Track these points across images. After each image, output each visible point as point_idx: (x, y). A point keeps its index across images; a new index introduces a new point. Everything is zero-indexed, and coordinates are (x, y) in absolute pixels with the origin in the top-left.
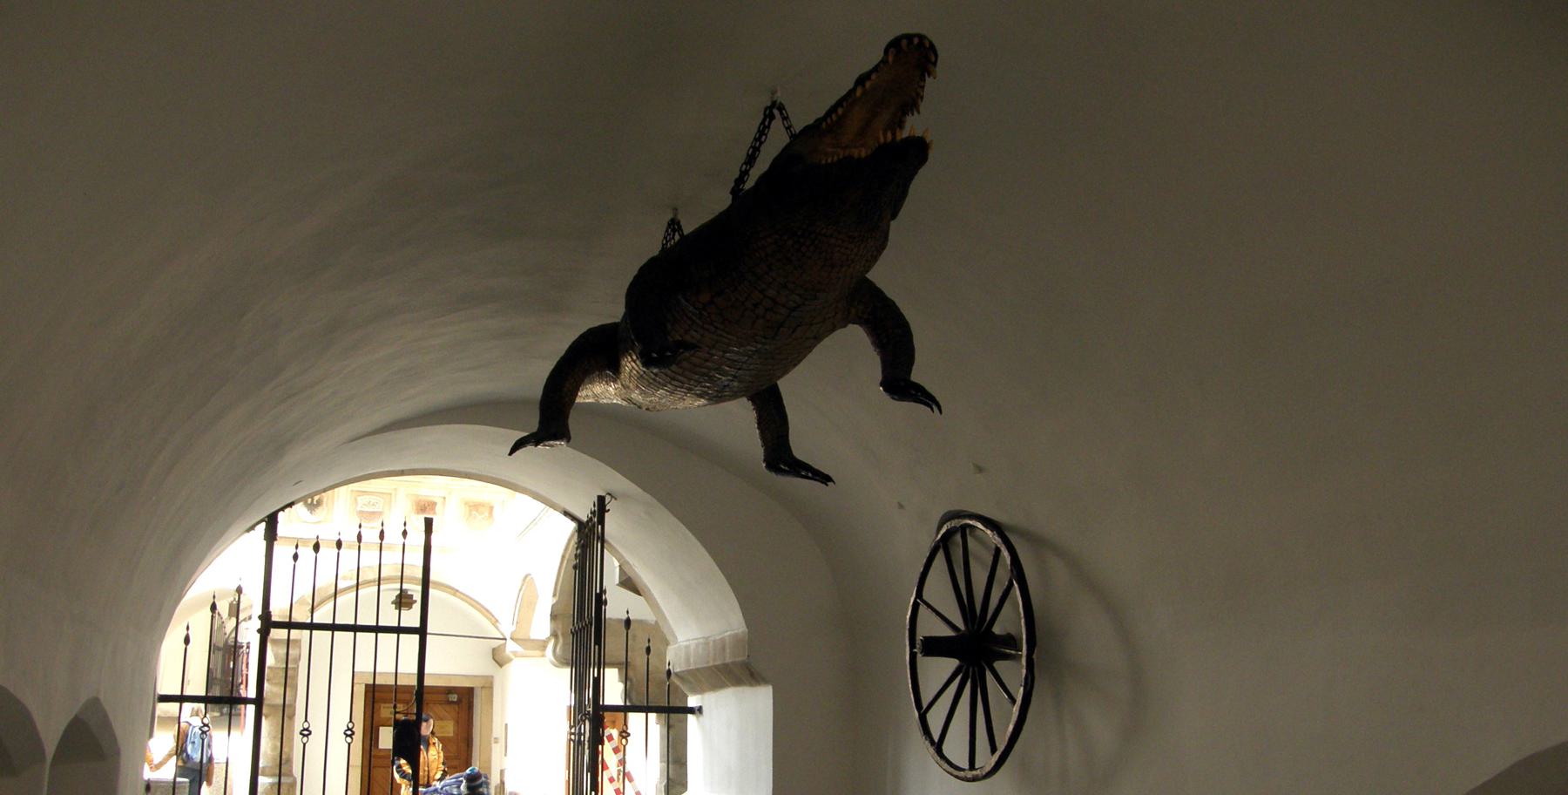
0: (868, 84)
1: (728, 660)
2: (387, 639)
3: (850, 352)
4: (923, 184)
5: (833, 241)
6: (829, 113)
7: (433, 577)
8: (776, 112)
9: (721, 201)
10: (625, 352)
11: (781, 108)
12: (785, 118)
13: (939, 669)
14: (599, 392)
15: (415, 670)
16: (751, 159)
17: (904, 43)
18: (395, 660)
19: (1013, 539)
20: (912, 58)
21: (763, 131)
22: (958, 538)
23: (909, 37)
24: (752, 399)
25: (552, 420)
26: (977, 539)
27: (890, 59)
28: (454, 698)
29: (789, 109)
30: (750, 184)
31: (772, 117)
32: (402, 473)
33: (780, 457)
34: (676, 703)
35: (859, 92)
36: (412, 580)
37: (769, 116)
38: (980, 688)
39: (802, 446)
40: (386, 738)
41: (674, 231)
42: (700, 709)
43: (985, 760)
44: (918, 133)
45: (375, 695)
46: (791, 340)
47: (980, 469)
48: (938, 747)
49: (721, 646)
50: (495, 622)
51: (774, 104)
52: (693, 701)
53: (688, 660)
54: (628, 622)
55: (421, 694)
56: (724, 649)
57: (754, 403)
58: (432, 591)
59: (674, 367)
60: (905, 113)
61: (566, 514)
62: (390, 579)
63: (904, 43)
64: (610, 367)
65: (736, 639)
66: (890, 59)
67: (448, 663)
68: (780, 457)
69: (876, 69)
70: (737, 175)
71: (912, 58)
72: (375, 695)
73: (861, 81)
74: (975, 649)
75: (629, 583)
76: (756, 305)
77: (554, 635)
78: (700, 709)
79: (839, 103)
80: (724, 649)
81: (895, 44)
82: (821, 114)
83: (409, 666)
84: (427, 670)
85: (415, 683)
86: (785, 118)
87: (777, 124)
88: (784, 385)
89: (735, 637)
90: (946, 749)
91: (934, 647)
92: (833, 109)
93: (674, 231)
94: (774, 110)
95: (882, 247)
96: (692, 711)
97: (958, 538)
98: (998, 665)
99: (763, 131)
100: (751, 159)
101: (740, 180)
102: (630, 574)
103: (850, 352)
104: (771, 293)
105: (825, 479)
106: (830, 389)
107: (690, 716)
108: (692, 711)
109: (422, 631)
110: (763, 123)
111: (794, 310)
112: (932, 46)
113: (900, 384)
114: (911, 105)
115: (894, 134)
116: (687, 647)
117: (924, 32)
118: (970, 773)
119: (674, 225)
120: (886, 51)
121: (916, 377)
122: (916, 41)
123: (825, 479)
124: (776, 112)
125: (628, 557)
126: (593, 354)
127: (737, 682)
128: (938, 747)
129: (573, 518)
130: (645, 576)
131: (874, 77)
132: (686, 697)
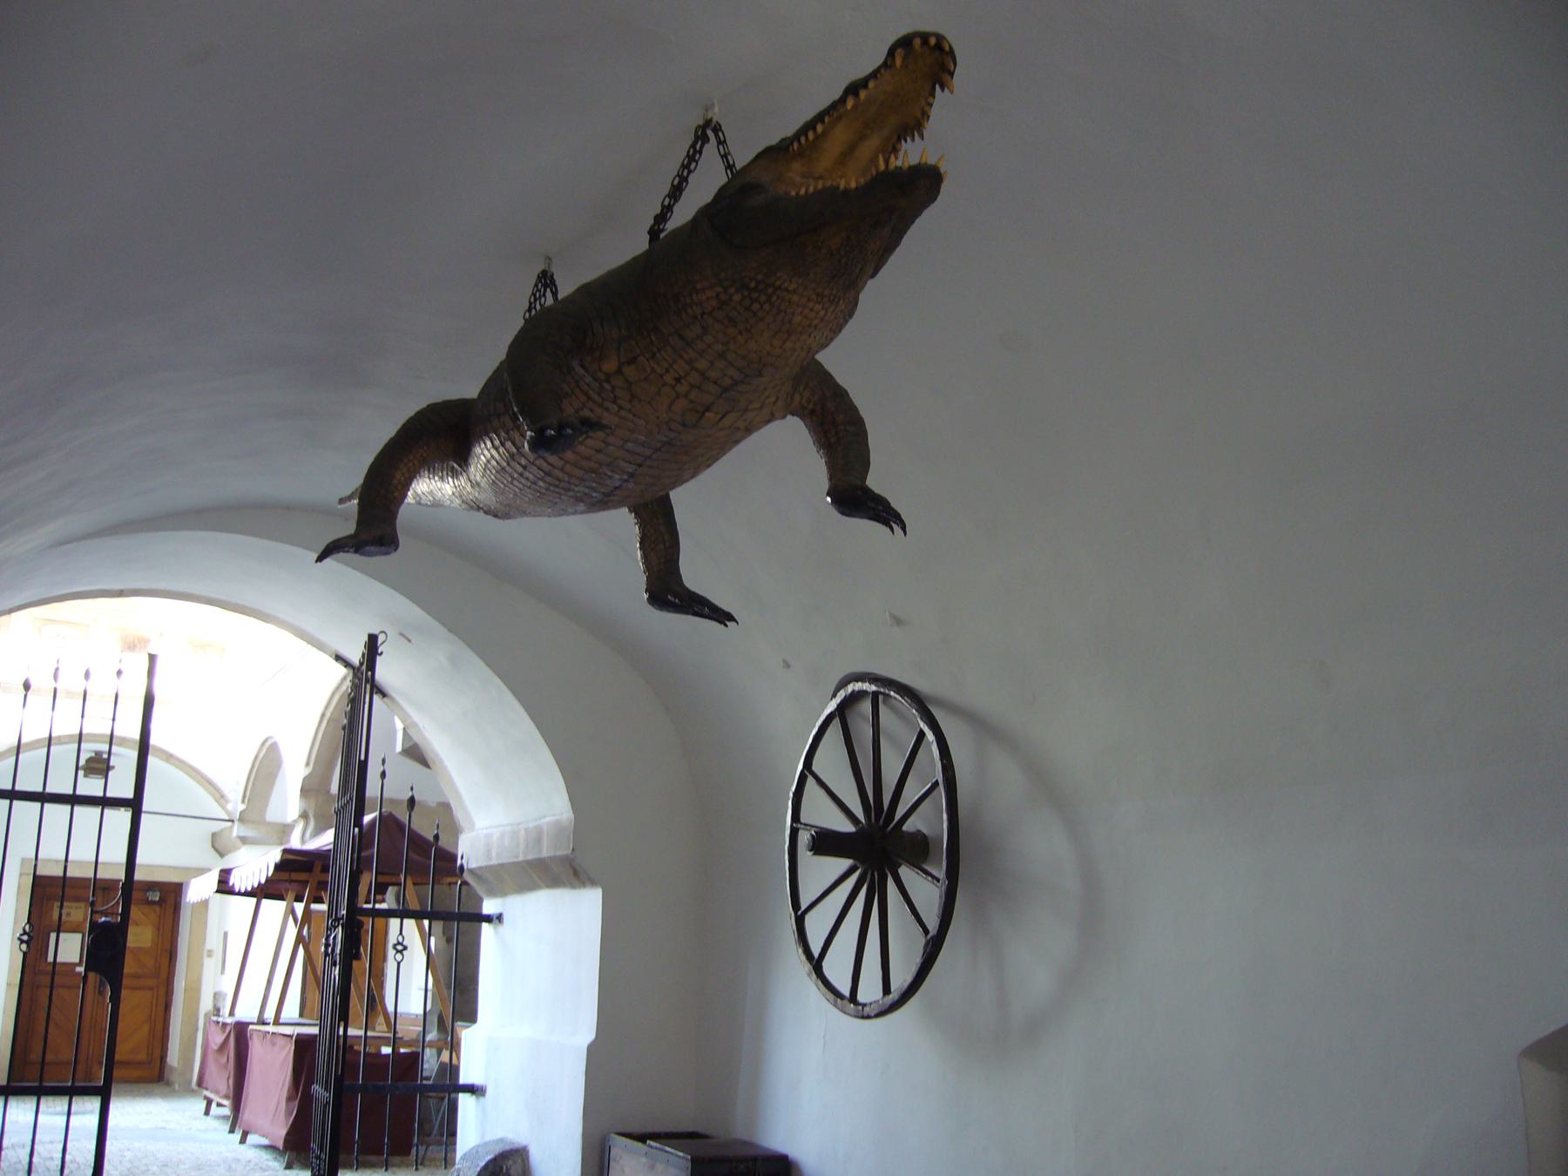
0: (863, 94)
1: (545, 853)
2: (87, 816)
3: (785, 452)
4: (927, 232)
5: (795, 298)
6: (797, 136)
7: (154, 740)
8: (710, 133)
9: (627, 244)
10: (480, 438)
11: (717, 129)
12: (721, 143)
13: (821, 871)
14: (431, 489)
15: (123, 858)
16: (676, 192)
17: (917, 42)
18: (91, 845)
19: (938, 714)
20: (924, 61)
21: (693, 157)
22: (866, 706)
23: (924, 37)
24: (635, 510)
25: (373, 527)
26: (892, 708)
27: (898, 62)
28: (155, 896)
29: (729, 132)
30: (682, 215)
31: (705, 140)
32: (121, 594)
33: (668, 591)
34: (50, 968)
35: (850, 103)
36: (124, 742)
37: (701, 137)
38: (877, 893)
39: (695, 574)
40: (70, 949)
41: (546, 286)
42: (500, 918)
43: (870, 990)
44: (931, 161)
45: (50, 895)
46: (697, 440)
47: (898, 622)
48: (817, 965)
49: (537, 836)
50: (220, 797)
51: (708, 123)
52: (489, 907)
53: (488, 852)
54: (412, 802)
55: (130, 888)
56: (539, 840)
57: (637, 515)
58: (152, 761)
59: (569, 455)
60: (899, 140)
61: (338, 658)
62: (63, 740)
63: (917, 42)
64: (456, 456)
65: (558, 828)
66: (898, 62)
67: (156, 858)
68: (668, 591)
69: (874, 75)
70: (658, 210)
71: (924, 61)
72: (50, 895)
73: (853, 89)
74: (876, 848)
75: (415, 753)
76: (678, 380)
77: (304, 815)
78: (500, 918)
79: (820, 117)
80: (539, 840)
81: (905, 43)
82: (789, 131)
83: (114, 853)
84: (139, 860)
85: (122, 876)
86: (721, 143)
87: (711, 150)
88: (676, 496)
89: (557, 824)
90: (827, 966)
91: (826, 843)
92: (810, 126)
93: (546, 286)
94: (707, 131)
95: (851, 314)
96: (488, 919)
97: (866, 706)
98: (905, 872)
99: (693, 157)
100: (676, 192)
101: (661, 218)
102: (416, 738)
103: (785, 452)
104: (702, 364)
105: (723, 617)
106: (752, 499)
107: (485, 926)
108: (488, 919)
109: (135, 804)
110: (693, 146)
111: (726, 390)
112: (951, 53)
113: (855, 498)
114: (913, 126)
115: (887, 162)
116: (488, 836)
117: (941, 32)
118: (850, 1000)
119: (546, 280)
120: (891, 53)
121: (874, 482)
122: (933, 41)
123: (723, 617)
124: (710, 133)
125: (416, 716)
126: (439, 436)
127: (554, 882)
128: (817, 965)
129: (347, 664)
130: (437, 742)
131: (871, 84)
132: (480, 901)
